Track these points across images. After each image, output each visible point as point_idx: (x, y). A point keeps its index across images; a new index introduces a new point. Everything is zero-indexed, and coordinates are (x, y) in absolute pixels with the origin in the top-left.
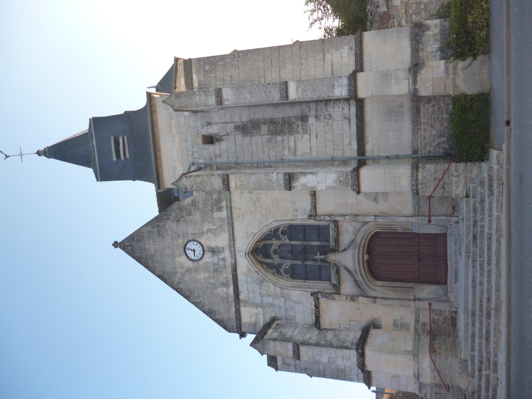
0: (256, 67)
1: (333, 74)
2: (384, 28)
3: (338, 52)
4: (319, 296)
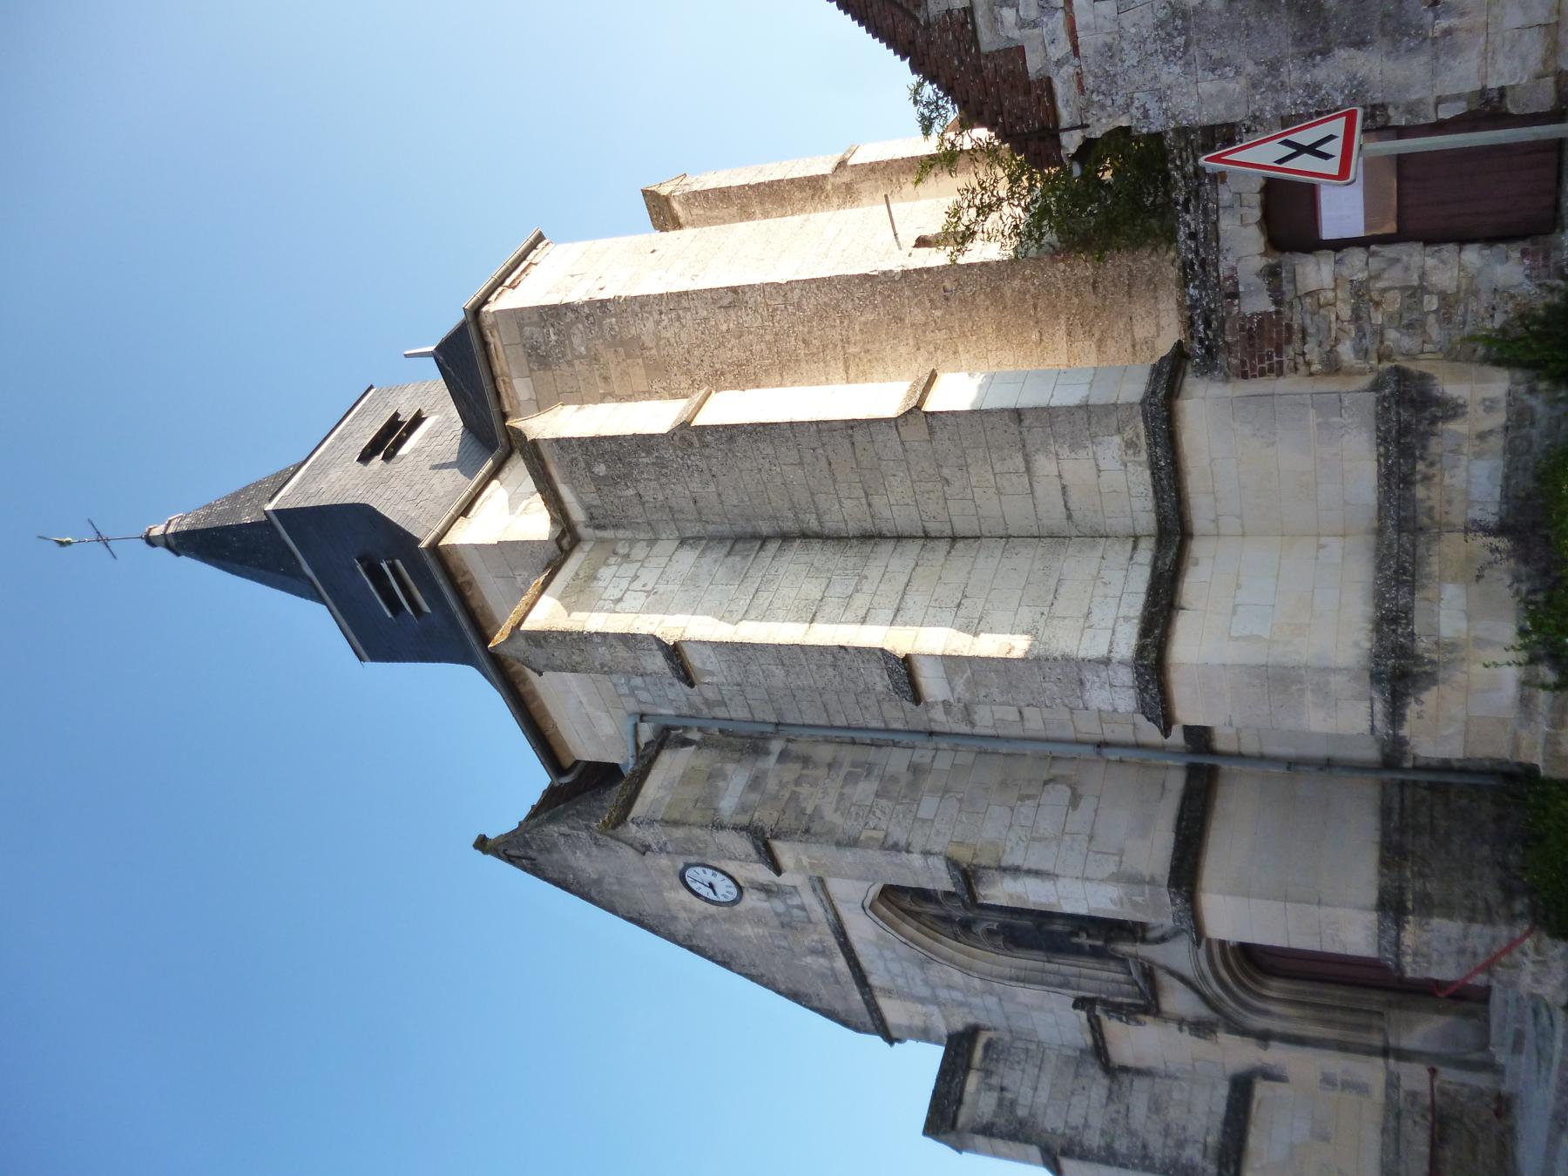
0: (779, 480)
1: (1069, 517)
2: (1262, 373)
3: (1082, 453)
4: (1098, 1010)
